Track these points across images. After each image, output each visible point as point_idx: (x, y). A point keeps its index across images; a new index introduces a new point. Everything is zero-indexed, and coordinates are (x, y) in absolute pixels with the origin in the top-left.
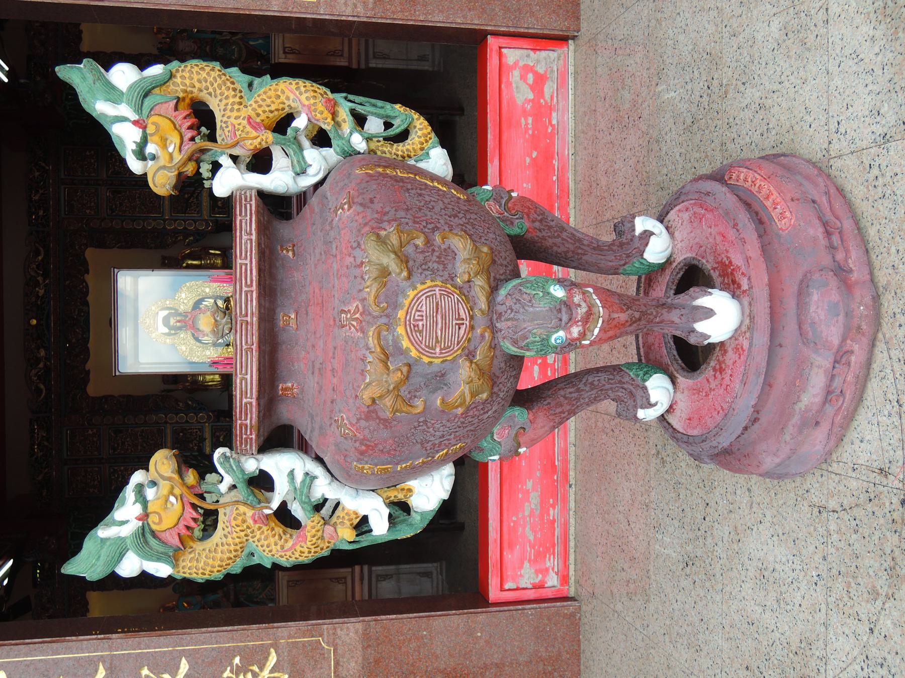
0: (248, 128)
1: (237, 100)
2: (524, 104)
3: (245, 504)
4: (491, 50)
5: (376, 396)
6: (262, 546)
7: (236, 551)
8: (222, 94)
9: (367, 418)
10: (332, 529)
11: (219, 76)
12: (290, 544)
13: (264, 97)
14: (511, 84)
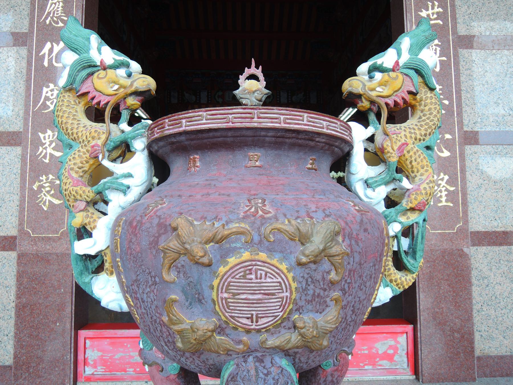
0: (399, 144)
1: (418, 137)
2: (375, 348)
3: (107, 139)
4: (405, 327)
5: (180, 230)
6: (74, 154)
7: (72, 134)
8: (421, 126)
9: (160, 225)
10: (83, 208)
11: (434, 124)
12: (74, 175)
13: (422, 157)
14: (386, 340)
